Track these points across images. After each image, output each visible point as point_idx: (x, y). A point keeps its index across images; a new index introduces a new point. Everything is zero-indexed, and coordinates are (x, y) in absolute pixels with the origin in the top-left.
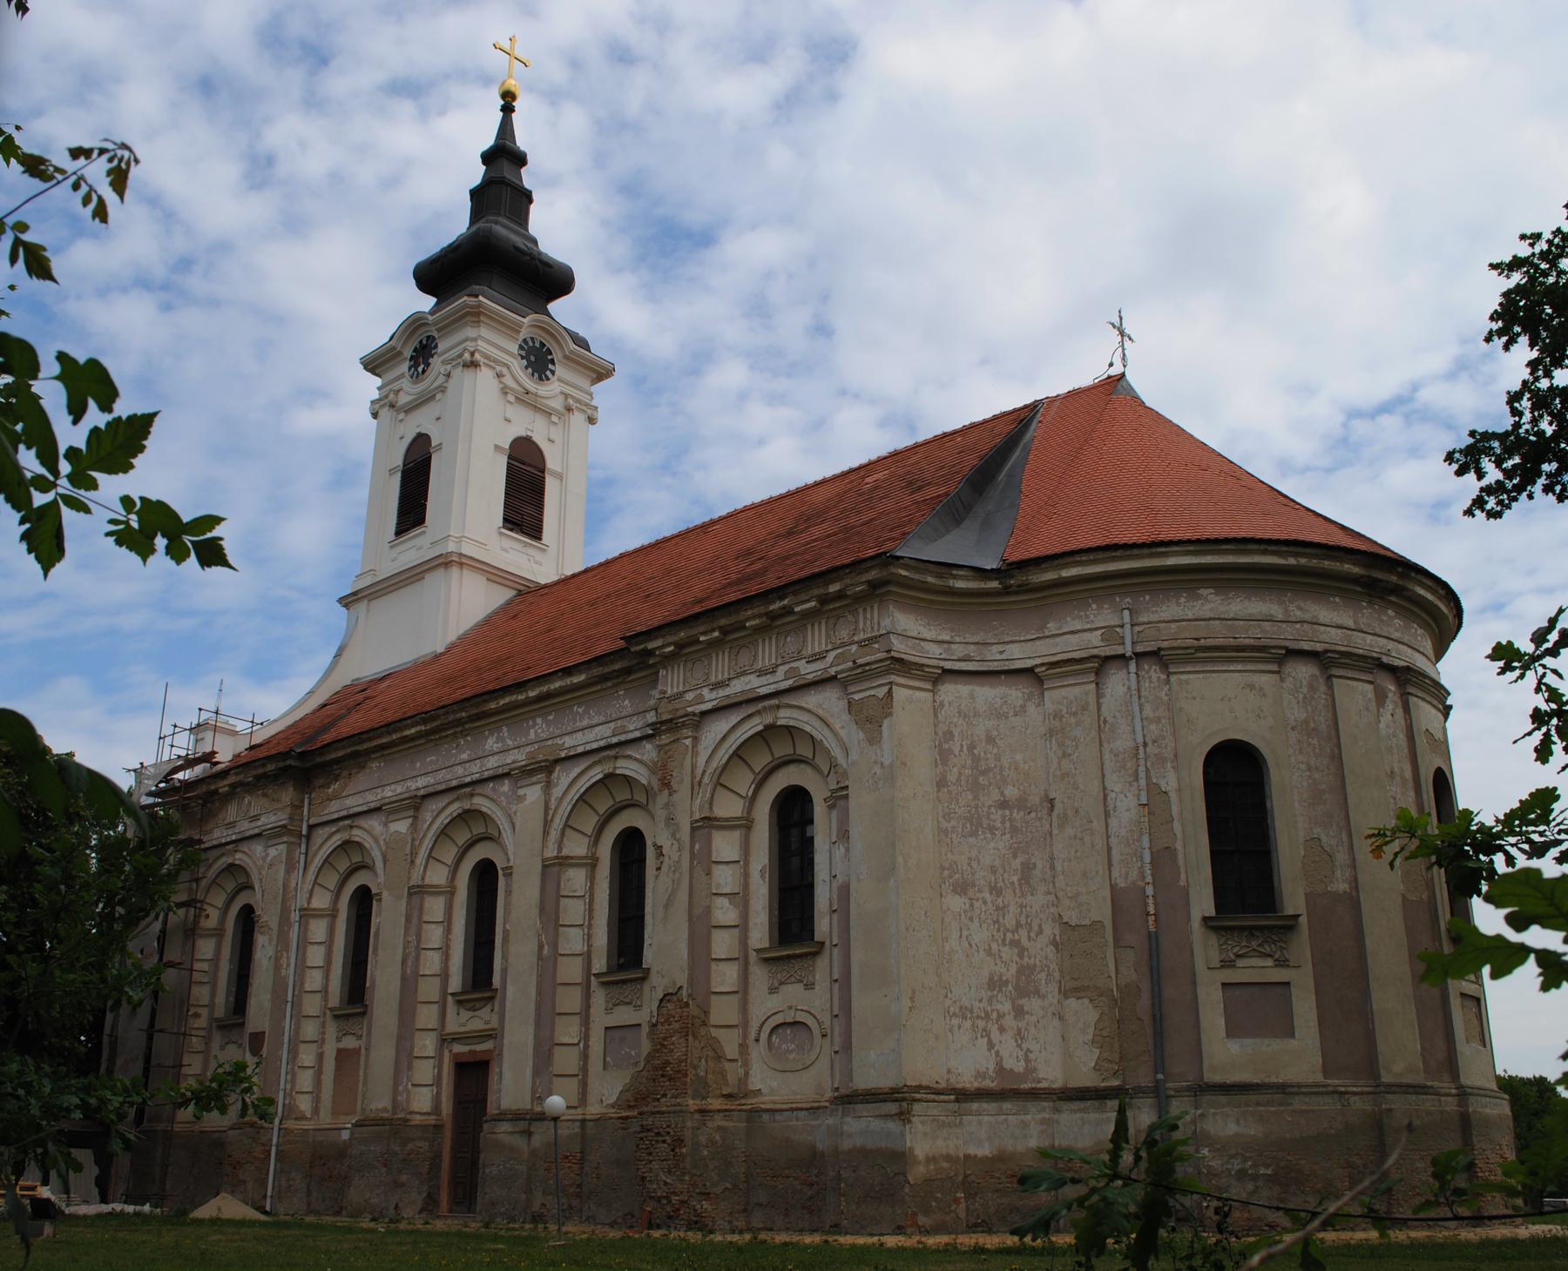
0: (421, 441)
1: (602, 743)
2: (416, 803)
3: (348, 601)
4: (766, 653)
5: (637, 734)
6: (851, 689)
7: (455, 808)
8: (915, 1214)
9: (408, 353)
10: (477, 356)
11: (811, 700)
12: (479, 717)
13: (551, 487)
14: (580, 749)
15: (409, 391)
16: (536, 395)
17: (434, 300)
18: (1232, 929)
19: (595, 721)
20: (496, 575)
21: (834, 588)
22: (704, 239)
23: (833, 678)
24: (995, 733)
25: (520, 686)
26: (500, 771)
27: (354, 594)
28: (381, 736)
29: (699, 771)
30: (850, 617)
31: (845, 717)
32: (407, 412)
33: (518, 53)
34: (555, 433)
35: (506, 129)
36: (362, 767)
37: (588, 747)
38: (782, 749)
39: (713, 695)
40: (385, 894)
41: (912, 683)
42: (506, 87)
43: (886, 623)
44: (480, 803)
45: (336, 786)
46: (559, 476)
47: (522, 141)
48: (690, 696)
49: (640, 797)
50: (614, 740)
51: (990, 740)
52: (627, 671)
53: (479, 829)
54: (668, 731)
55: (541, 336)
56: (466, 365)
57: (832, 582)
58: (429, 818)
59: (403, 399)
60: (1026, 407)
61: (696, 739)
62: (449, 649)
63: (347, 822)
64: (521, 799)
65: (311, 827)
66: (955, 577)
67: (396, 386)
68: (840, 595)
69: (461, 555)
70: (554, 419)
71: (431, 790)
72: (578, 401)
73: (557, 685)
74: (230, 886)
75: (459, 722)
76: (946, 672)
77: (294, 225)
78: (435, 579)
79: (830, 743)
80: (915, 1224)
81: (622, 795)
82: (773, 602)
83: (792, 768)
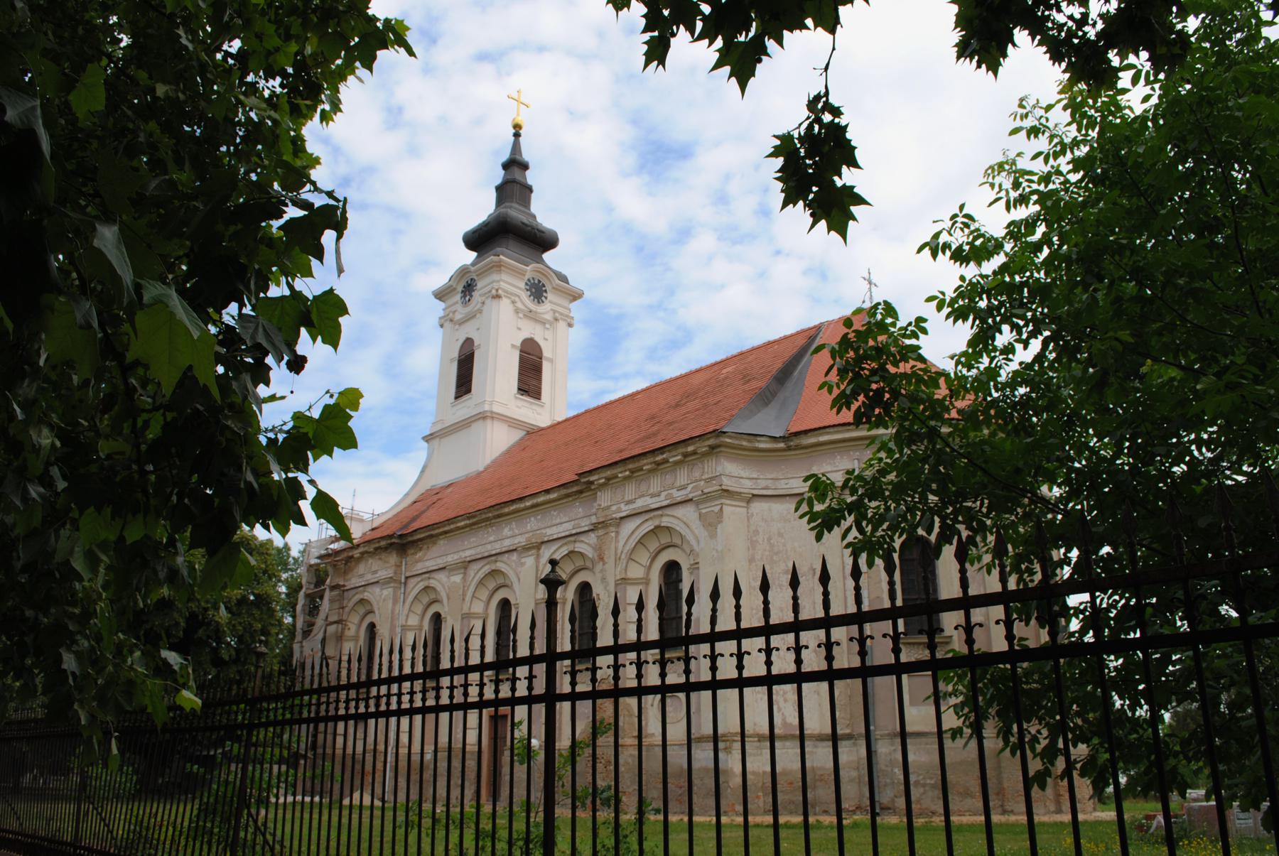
0: (469, 341)
1: (567, 533)
2: (466, 565)
3: (428, 438)
4: (655, 484)
5: (586, 529)
6: (701, 507)
7: (487, 569)
8: (733, 805)
9: (460, 288)
10: (500, 292)
11: (680, 512)
12: (499, 516)
13: (546, 367)
14: (555, 537)
15: (461, 312)
16: (536, 312)
17: (475, 254)
18: (914, 644)
19: (564, 520)
20: (513, 423)
21: (690, 449)
22: (683, 153)
23: (691, 500)
24: (783, 531)
25: (521, 499)
26: (511, 548)
27: (431, 435)
28: (444, 526)
29: (619, 551)
30: (700, 465)
31: (698, 522)
32: (460, 324)
33: (522, 100)
34: (548, 334)
35: (516, 147)
36: (435, 543)
37: (560, 535)
38: (665, 540)
39: (627, 508)
40: (448, 618)
41: (734, 503)
42: (516, 121)
43: (719, 469)
44: (500, 566)
45: (420, 554)
46: (551, 361)
47: (526, 155)
48: (614, 508)
49: (589, 564)
50: (574, 532)
51: (780, 535)
52: (581, 492)
53: (500, 581)
54: (602, 528)
55: (538, 276)
56: (494, 297)
57: (689, 445)
58: (472, 575)
59: (458, 317)
60: (815, 327)
61: (617, 533)
62: (487, 468)
63: (427, 575)
64: (523, 564)
65: (407, 578)
66: (759, 441)
67: (453, 308)
68: (694, 453)
69: (492, 412)
70: (547, 326)
71: (473, 558)
72: (561, 314)
73: (541, 499)
74: (362, 611)
75: (488, 519)
76: (754, 495)
77: (413, 151)
78: (477, 427)
79: (690, 537)
80: (734, 810)
81: (579, 563)
82: (658, 455)
83: (671, 550)
